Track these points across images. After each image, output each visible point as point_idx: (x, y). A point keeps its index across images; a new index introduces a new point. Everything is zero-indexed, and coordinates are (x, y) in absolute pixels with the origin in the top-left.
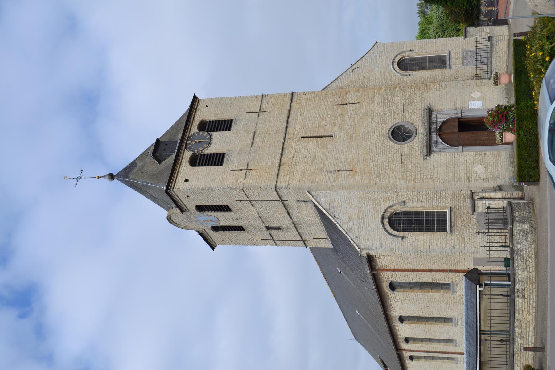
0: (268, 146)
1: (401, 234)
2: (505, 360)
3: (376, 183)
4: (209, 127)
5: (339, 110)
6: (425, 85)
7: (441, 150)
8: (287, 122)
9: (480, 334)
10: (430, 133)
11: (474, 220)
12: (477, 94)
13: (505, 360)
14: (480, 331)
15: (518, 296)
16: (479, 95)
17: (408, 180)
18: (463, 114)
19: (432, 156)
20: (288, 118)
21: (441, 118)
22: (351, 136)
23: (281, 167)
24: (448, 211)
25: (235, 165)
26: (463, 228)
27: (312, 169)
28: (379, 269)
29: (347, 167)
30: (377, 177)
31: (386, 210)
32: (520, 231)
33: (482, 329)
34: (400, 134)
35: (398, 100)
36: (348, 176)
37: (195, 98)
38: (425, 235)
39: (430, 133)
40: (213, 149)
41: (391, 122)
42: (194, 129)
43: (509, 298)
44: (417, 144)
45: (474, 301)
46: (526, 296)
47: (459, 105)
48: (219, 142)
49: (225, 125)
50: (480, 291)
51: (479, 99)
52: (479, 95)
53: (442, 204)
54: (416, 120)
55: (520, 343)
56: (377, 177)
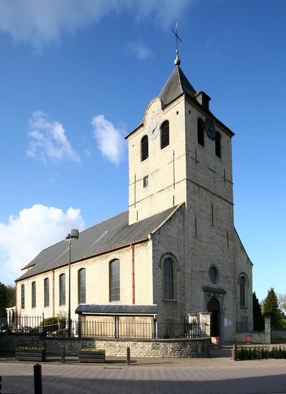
0: (208, 180)
1: (162, 266)
2: (100, 334)
3: (190, 252)
4: (217, 139)
5: (225, 234)
6: (235, 292)
7: (206, 298)
8: (220, 197)
9: (116, 316)
10: (214, 292)
11: (170, 318)
12: (230, 323)
13: (100, 334)
14: (118, 316)
15: (153, 344)
16: (230, 325)
17: (191, 274)
18: (222, 314)
19: (203, 292)
20: (222, 198)
21: (220, 300)
22: (212, 239)
23: (197, 186)
24: (174, 300)
25: (199, 153)
26: (166, 309)
27: (197, 209)
28: (54, 272)
29: (198, 233)
30: (193, 254)
31: (175, 257)
32: (198, 346)
33: (120, 317)
34: (214, 271)
35: (229, 274)
36: (193, 233)
37: (148, 176)
38: (162, 283)
39: (214, 292)
40: (206, 139)
41: (219, 266)
42: (217, 129)
43: (114, 337)
44: (208, 283)
45: (144, 311)
46: (153, 350)
47: (226, 312)
48: (210, 144)
49: (218, 153)
50: (153, 316)
51: (228, 325)
52: (230, 325)
53: (178, 296)
54: (221, 284)
55: (116, 345)
56: (193, 254)
